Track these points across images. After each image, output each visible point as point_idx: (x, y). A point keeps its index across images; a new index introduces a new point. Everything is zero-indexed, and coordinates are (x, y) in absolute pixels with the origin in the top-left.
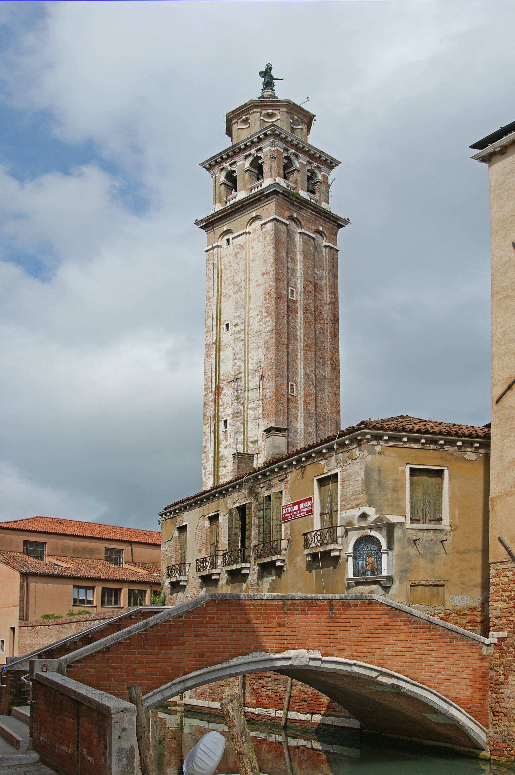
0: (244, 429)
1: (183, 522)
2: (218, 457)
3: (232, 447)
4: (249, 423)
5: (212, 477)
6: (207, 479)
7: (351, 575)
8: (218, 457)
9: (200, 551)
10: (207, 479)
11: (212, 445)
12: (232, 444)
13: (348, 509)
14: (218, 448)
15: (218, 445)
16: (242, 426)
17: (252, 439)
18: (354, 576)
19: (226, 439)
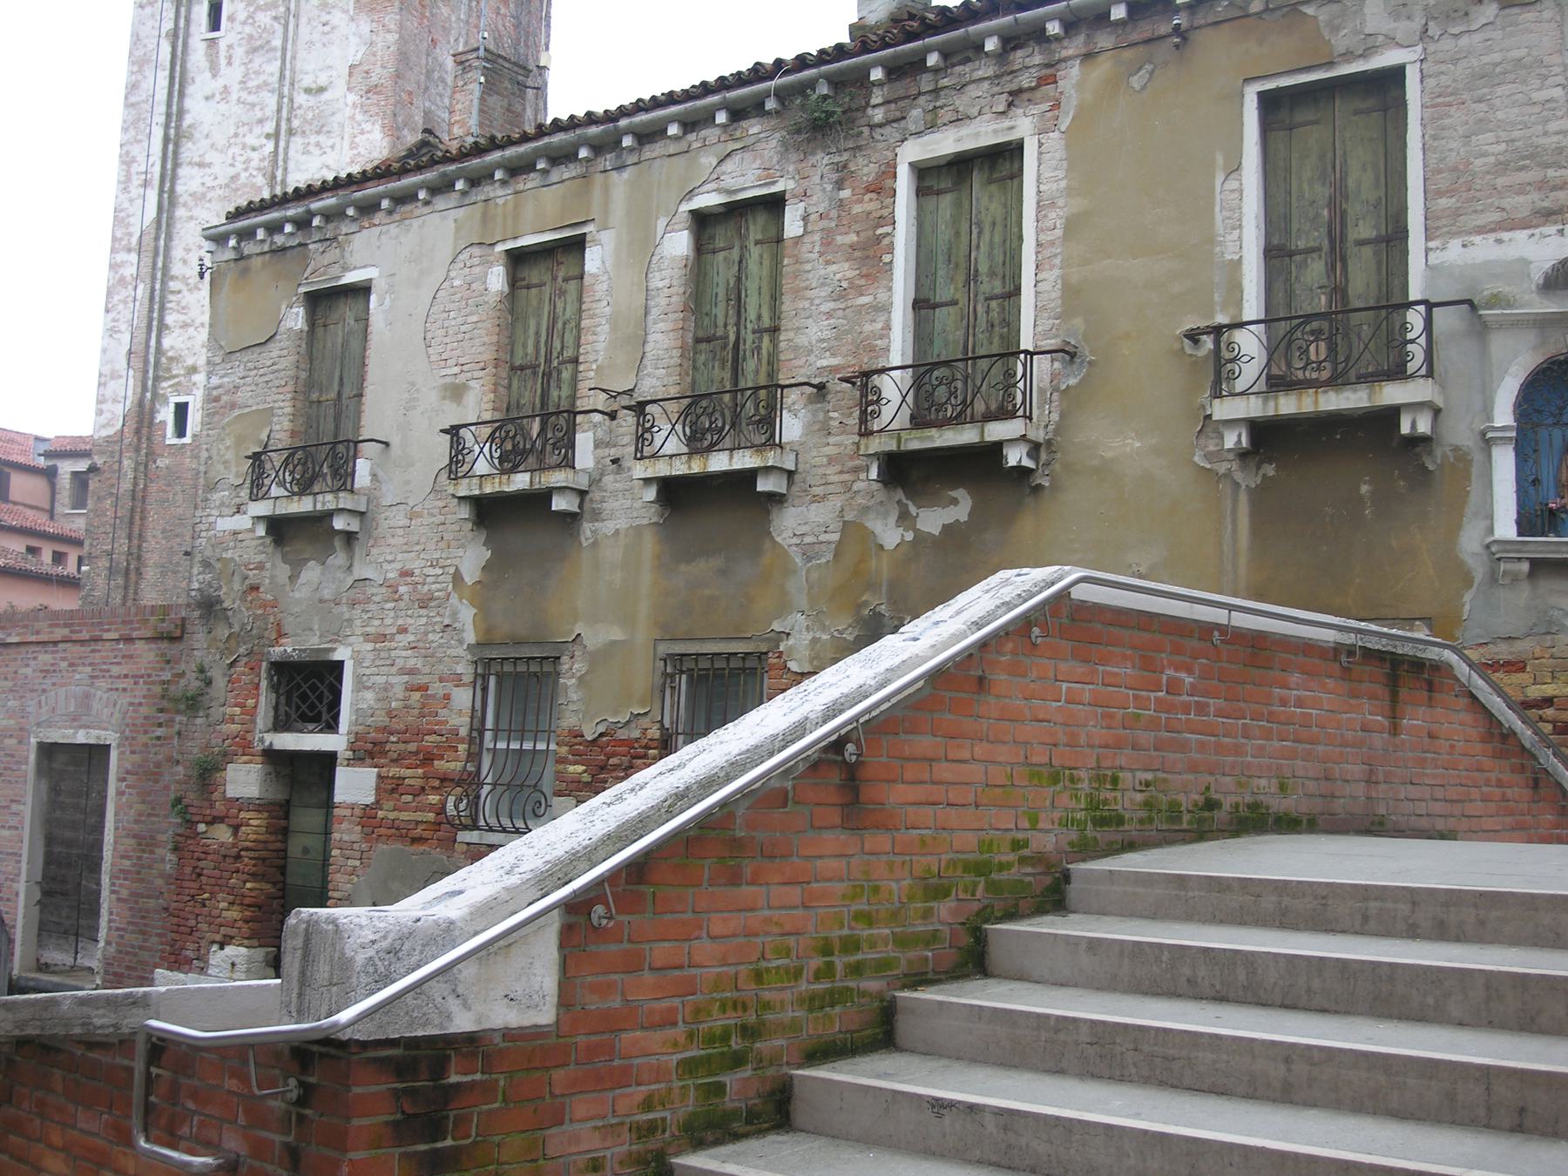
0: (285, 40)
1: (346, 269)
2: (178, 128)
3: (234, 97)
4: (303, 20)
5: (152, 196)
6: (131, 201)
7: (1506, 527)
8: (178, 128)
9: (456, 392)
10: (131, 201)
11: (163, 82)
12: (235, 88)
13: (1480, 230)
14: (182, 94)
15: (181, 85)
16: (279, 28)
17: (307, 81)
18: (1520, 534)
19: (214, 70)
